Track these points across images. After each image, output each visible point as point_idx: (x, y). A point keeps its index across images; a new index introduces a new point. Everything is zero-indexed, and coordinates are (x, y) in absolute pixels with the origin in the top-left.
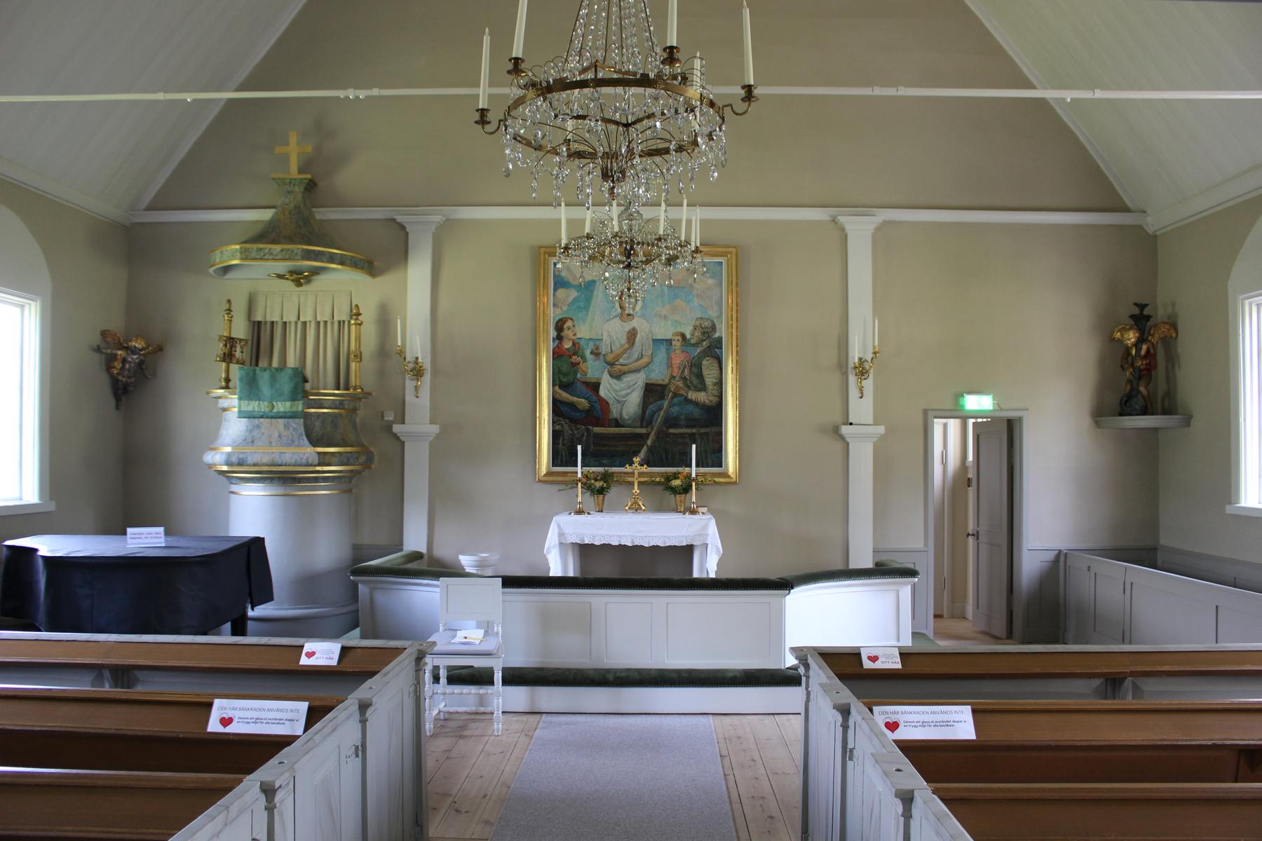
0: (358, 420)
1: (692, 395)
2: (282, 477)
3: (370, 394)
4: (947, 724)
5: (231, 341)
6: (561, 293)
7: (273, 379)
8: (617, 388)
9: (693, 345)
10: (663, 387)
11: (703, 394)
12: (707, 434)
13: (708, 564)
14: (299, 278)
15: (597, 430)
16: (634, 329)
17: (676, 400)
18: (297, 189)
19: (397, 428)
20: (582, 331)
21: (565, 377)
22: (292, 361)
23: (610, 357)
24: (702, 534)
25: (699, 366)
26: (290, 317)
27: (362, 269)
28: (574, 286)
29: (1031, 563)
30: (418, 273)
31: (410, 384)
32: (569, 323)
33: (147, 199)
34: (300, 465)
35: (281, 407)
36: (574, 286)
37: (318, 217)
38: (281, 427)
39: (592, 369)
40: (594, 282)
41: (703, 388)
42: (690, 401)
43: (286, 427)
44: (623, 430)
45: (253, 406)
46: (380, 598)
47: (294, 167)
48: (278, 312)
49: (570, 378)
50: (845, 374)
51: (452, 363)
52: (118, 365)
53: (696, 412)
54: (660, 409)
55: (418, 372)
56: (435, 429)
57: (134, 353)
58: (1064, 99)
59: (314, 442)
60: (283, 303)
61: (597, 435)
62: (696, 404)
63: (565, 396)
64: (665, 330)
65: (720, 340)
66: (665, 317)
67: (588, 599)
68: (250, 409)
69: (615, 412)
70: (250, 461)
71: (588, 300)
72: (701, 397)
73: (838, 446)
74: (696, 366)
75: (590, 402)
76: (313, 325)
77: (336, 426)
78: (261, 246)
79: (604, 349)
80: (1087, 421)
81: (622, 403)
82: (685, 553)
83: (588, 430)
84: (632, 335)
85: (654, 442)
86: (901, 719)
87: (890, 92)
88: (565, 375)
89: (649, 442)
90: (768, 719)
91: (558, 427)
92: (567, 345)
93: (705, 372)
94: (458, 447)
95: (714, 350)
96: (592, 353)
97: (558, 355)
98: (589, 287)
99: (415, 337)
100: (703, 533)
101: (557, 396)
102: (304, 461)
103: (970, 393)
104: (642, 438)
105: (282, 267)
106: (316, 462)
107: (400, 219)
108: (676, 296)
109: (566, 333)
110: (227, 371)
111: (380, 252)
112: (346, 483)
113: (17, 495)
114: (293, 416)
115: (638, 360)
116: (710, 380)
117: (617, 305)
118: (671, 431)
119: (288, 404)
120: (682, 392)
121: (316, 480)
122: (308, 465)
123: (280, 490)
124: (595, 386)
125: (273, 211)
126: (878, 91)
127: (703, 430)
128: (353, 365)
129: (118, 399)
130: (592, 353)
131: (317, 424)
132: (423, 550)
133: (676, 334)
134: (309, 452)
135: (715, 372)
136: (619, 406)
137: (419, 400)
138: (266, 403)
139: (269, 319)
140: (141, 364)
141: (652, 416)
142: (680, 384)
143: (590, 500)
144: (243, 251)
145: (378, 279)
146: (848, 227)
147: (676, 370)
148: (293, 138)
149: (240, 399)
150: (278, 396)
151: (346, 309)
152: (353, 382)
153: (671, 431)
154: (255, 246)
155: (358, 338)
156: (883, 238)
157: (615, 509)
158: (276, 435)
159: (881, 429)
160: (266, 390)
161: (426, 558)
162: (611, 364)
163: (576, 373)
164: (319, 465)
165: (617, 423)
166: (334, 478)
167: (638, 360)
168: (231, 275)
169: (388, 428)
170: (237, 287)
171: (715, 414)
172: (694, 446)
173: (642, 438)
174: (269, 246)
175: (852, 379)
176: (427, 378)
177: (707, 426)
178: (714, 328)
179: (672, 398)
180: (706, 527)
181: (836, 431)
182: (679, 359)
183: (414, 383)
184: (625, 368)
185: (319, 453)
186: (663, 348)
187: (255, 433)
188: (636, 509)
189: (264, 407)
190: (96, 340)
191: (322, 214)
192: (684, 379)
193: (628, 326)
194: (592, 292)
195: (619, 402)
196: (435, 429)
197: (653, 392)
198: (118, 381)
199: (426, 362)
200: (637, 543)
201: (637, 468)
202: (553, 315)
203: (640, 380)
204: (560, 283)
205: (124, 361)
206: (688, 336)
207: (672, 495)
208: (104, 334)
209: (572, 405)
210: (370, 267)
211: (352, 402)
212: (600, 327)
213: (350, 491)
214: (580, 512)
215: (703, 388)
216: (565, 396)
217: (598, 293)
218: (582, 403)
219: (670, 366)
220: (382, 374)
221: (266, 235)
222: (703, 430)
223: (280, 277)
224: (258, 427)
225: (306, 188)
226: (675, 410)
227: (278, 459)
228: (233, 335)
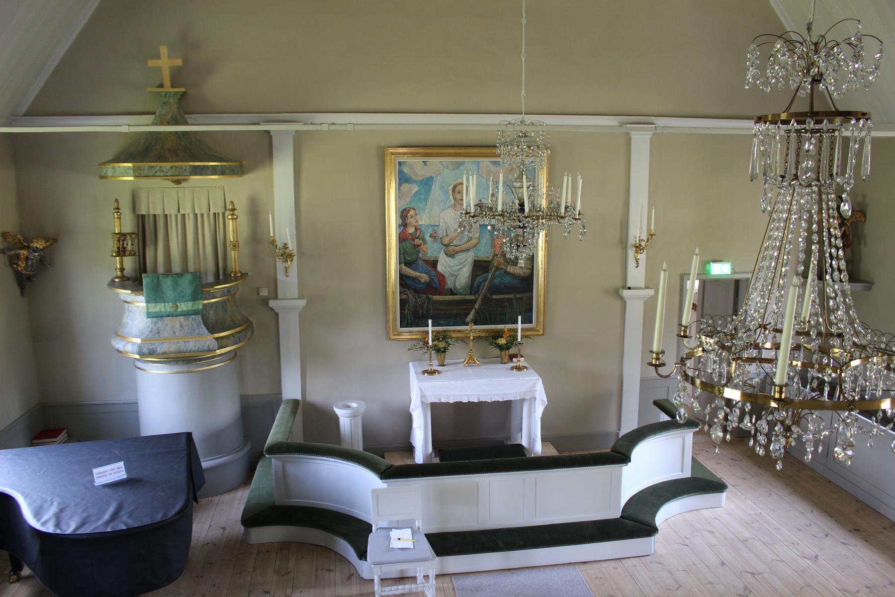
2: (182, 359)
3: (247, 274)
6: (405, 187)
7: (175, 285)
8: (452, 265)
12: (521, 298)
15: (436, 298)
17: (497, 273)
18: (171, 100)
19: (272, 303)
20: (423, 220)
26: (171, 211)
28: (416, 182)
30: (282, 172)
31: (280, 265)
32: (412, 212)
35: (184, 307)
36: (416, 182)
39: (431, 250)
42: (507, 273)
45: (160, 307)
46: (291, 469)
47: (167, 83)
49: (414, 257)
50: (625, 248)
51: (313, 245)
52: (22, 264)
53: (515, 282)
54: (485, 281)
55: (287, 256)
57: (35, 251)
61: (435, 302)
62: (514, 276)
63: (409, 271)
68: (157, 310)
69: (450, 284)
70: (159, 350)
71: (428, 192)
73: (618, 303)
75: (429, 276)
76: (192, 216)
78: (152, 164)
79: (440, 234)
85: (480, 306)
89: (476, 306)
90: (617, 564)
91: (404, 297)
92: (411, 230)
96: (431, 236)
98: (427, 183)
99: (282, 226)
100: (532, 390)
101: (404, 272)
102: (206, 348)
103: (714, 261)
104: (472, 302)
109: (409, 220)
110: (122, 263)
117: (451, 198)
118: (494, 297)
119: (190, 304)
120: (503, 267)
123: (184, 368)
124: (434, 264)
127: (518, 296)
129: (22, 287)
130: (431, 236)
131: (212, 312)
134: (209, 340)
136: (453, 278)
137: (289, 279)
138: (170, 304)
139: (152, 212)
141: (479, 286)
142: (501, 260)
144: (135, 169)
145: (246, 177)
148: (164, 51)
149: (147, 302)
150: (181, 298)
151: (221, 203)
153: (494, 297)
160: (169, 293)
162: (447, 246)
163: (418, 253)
165: (452, 292)
167: (468, 241)
169: (265, 301)
173: (472, 302)
176: (295, 258)
177: (520, 293)
179: (495, 271)
180: (534, 385)
181: (617, 293)
183: (284, 265)
185: (217, 339)
187: (159, 325)
188: (470, 362)
194: (430, 186)
196: (303, 303)
197: (480, 267)
198: (21, 274)
199: (295, 252)
212: (439, 217)
216: (409, 271)
218: (424, 278)
219: (493, 246)
220: (255, 256)
222: (518, 296)
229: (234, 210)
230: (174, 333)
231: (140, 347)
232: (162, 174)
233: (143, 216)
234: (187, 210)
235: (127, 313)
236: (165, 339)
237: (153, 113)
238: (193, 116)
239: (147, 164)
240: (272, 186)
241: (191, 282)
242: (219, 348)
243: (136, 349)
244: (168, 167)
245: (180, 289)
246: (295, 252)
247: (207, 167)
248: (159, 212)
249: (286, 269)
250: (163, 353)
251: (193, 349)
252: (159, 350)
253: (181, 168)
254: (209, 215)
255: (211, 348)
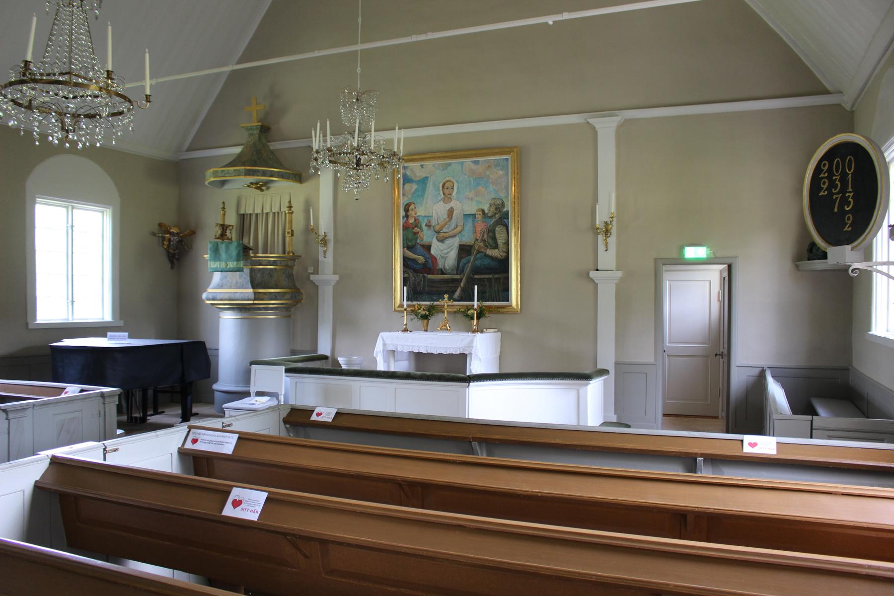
0: (294, 273)
1: (489, 252)
4: (221, 443)
5: (224, 227)
6: (408, 186)
7: (227, 248)
9: (490, 217)
10: (471, 247)
11: (496, 250)
12: (498, 279)
13: (475, 367)
14: (260, 187)
15: (430, 276)
16: (452, 208)
17: (478, 255)
18: (255, 132)
19: (312, 277)
20: (420, 211)
21: (410, 244)
23: (437, 228)
24: (482, 350)
25: (494, 232)
27: (288, 178)
29: (739, 379)
31: (321, 249)
32: (412, 206)
33: (187, 145)
35: (232, 265)
37: (272, 148)
39: (426, 236)
40: (427, 178)
41: (496, 247)
42: (487, 256)
44: (446, 277)
48: (252, 207)
49: (414, 243)
53: (494, 264)
54: (469, 262)
56: (336, 277)
58: (547, 23)
60: (257, 203)
64: (472, 208)
65: (507, 213)
66: (472, 199)
67: (351, 383)
69: (440, 265)
71: (424, 190)
72: (495, 253)
74: (491, 231)
75: (425, 258)
77: (271, 276)
79: (433, 223)
80: (788, 265)
81: (445, 258)
82: (462, 358)
83: (424, 277)
84: (451, 212)
85: (465, 284)
86: (200, 437)
87: (423, 37)
88: (410, 241)
89: (462, 285)
91: (406, 275)
92: (411, 221)
93: (497, 236)
94: (351, 288)
95: (502, 220)
97: (406, 227)
98: (424, 181)
101: (406, 255)
108: (478, 184)
109: (411, 213)
112: (287, 311)
113: (101, 317)
114: (239, 270)
115: (454, 229)
116: (501, 241)
118: (476, 277)
119: (235, 263)
121: (259, 309)
123: (245, 315)
124: (428, 248)
126: (431, 36)
127: (497, 276)
128: (287, 239)
129: (172, 262)
131: (259, 275)
132: (328, 354)
133: (478, 210)
135: (504, 235)
137: (327, 260)
140: (180, 241)
141: (464, 267)
142: (482, 244)
143: (419, 323)
145: (304, 185)
146: (597, 126)
147: (479, 235)
150: (229, 258)
152: (287, 249)
153: (476, 277)
154: (232, 169)
155: (291, 222)
156: (624, 133)
157: (433, 330)
159: (619, 274)
160: (223, 255)
161: (330, 359)
162: (438, 232)
163: (417, 239)
164: (255, 300)
165: (442, 272)
167: (454, 229)
168: (226, 187)
169: (309, 277)
171: (504, 264)
172: (476, 287)
175: (601, 238)
176: (331, 245)
178: (503, 205)
182: (481, 227)
184: (446, 235)
186: (470, 220)
189: (223, 265)
190: (155, 228)
191: (274, 146)
192: (484, 241)
193: (448, 206)
194: (426, 184)
195: (443, 257)
196: (336, 277)
197: (464, 250)
199: (331, 236)
200: (429, 351)
201: (445, 302)
202: (403, 201)
203: (455, 243)
204: (407, 180)
205: (170, 240)
206: (486, 211)
207: (474, 320)
208: (160, 225)
209: (414, 260)
210: (299, 177)
211: (290, 261)
212: (431, 208)
213: (290, 316)
214: (405, 330)
215: (496, 247)
217: (430, 185)
218: (421, 259)
219: (475, 232)
220: (307, 243)
221: (237, 161)
222: (497, 276)
225: (261, 131)
226: (478, 263)
228: (226, 223)
241: (237, 247)
246: (331, 236)
247: (258, 171)
249: (325, 252)
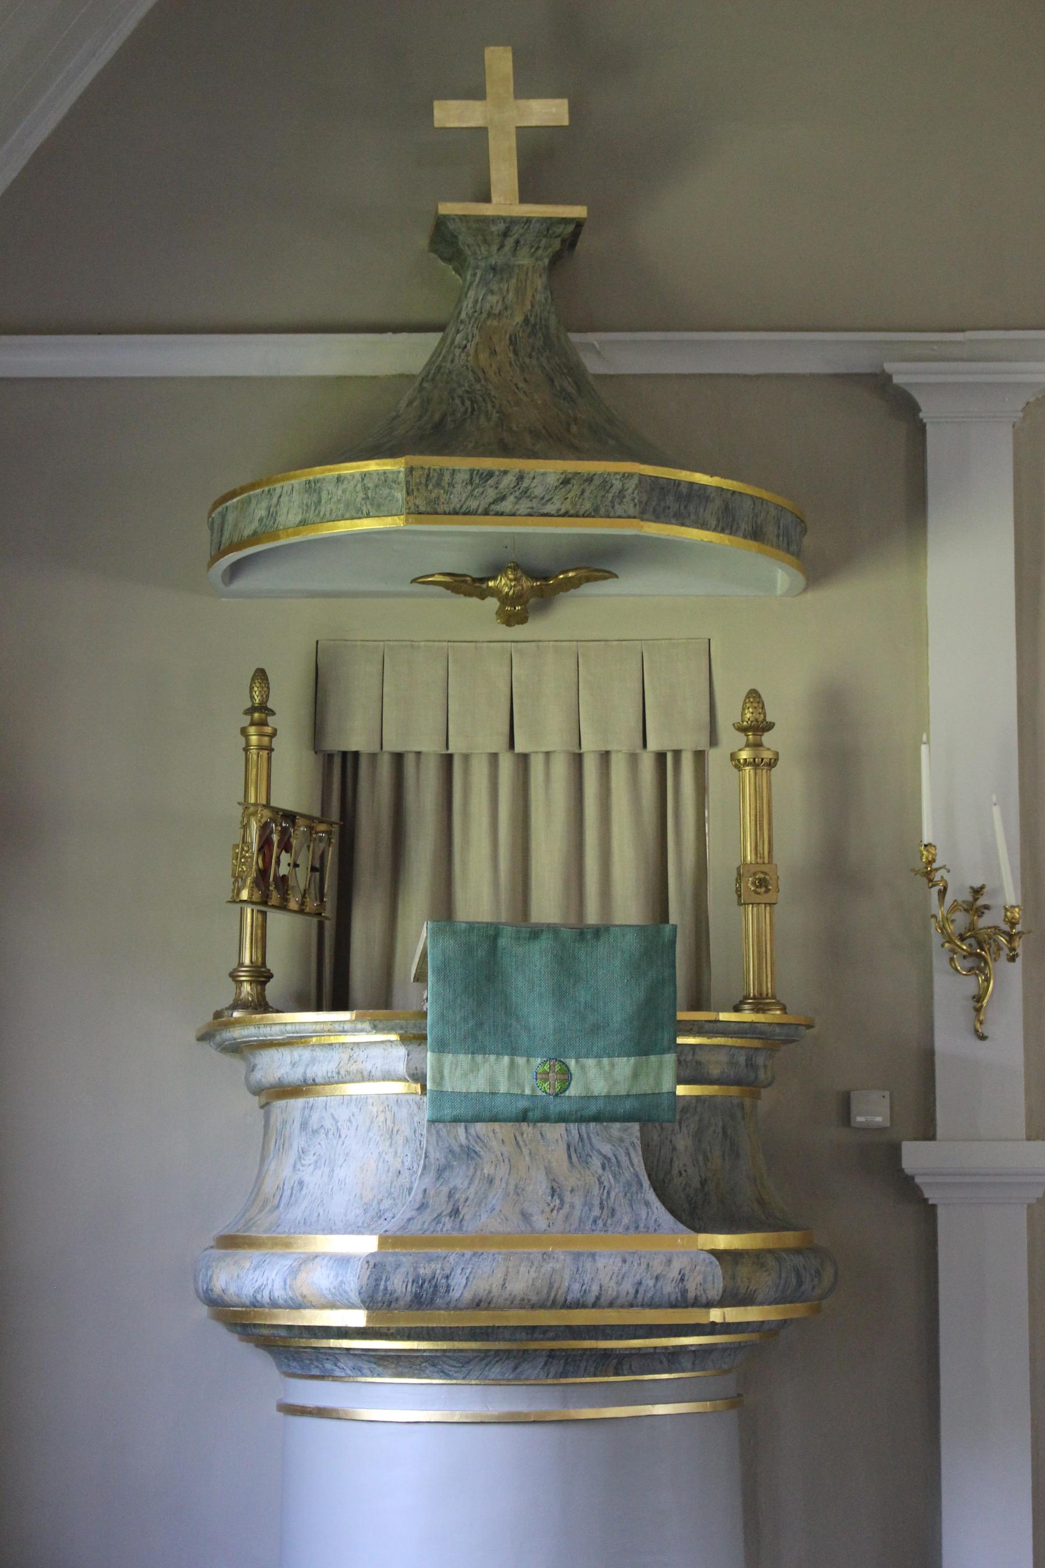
22: (479, 899)
26: (477, 736)
31: (951, 989)
34: (651, 1305)
35: (598, 1077)
38: (559, 1154)
43: (578, 1153)
59: (694, 1212)
60: (442, 685)
68: (478, 1084)
70: (460, 1289)
76: (560, 768)
99: (957, 805)
102: (669, 1288)
105: (458, 541)
106: (715, 1291)
107: (902, 374)
111: (842, 489)
112: (741, 1372)
119: (624, 1065)
121: (619, 1362)
122: (683, 1302)
125: (437, 336)
131: (683, 1142)
150: (590, 1035)
151: (695, 709)
158: (539, 1186)
160: (538, 1013)
166: (700, 1354)
170: (274, 624)
174: (516, 464)
183: (970, 985)
187: (458, 1179)
220: (835, 949)
223: (463, 585)
224: (469, 1153)
227: (569, 1285)
229: (760, 727)
230: (525, 1216)
231: (376, 1266)
232: (524, 506)
233: (350, 760)
234: (545, 735)
235: (298, 1142)
236: (483, 1240)
237: (440, 328)
238: (592, 337)
239: (462, 464)
240: (919, 638)
242: (721, 1303)
243: (353, 1282)
244: (552, 480)
245: (583, 995)
248: (429, 745)
250: (477, 1304)
251: (611, 1289)
252: (460, 1289)
253: (605, 483)
254: (633, 759)
255: (692, 1288)
